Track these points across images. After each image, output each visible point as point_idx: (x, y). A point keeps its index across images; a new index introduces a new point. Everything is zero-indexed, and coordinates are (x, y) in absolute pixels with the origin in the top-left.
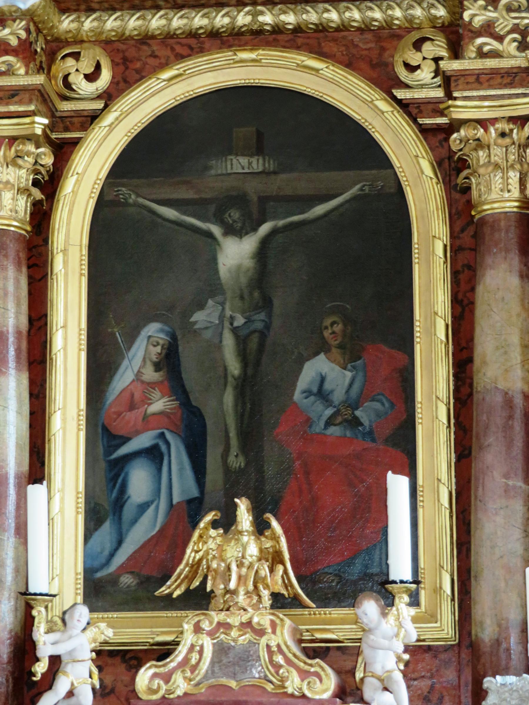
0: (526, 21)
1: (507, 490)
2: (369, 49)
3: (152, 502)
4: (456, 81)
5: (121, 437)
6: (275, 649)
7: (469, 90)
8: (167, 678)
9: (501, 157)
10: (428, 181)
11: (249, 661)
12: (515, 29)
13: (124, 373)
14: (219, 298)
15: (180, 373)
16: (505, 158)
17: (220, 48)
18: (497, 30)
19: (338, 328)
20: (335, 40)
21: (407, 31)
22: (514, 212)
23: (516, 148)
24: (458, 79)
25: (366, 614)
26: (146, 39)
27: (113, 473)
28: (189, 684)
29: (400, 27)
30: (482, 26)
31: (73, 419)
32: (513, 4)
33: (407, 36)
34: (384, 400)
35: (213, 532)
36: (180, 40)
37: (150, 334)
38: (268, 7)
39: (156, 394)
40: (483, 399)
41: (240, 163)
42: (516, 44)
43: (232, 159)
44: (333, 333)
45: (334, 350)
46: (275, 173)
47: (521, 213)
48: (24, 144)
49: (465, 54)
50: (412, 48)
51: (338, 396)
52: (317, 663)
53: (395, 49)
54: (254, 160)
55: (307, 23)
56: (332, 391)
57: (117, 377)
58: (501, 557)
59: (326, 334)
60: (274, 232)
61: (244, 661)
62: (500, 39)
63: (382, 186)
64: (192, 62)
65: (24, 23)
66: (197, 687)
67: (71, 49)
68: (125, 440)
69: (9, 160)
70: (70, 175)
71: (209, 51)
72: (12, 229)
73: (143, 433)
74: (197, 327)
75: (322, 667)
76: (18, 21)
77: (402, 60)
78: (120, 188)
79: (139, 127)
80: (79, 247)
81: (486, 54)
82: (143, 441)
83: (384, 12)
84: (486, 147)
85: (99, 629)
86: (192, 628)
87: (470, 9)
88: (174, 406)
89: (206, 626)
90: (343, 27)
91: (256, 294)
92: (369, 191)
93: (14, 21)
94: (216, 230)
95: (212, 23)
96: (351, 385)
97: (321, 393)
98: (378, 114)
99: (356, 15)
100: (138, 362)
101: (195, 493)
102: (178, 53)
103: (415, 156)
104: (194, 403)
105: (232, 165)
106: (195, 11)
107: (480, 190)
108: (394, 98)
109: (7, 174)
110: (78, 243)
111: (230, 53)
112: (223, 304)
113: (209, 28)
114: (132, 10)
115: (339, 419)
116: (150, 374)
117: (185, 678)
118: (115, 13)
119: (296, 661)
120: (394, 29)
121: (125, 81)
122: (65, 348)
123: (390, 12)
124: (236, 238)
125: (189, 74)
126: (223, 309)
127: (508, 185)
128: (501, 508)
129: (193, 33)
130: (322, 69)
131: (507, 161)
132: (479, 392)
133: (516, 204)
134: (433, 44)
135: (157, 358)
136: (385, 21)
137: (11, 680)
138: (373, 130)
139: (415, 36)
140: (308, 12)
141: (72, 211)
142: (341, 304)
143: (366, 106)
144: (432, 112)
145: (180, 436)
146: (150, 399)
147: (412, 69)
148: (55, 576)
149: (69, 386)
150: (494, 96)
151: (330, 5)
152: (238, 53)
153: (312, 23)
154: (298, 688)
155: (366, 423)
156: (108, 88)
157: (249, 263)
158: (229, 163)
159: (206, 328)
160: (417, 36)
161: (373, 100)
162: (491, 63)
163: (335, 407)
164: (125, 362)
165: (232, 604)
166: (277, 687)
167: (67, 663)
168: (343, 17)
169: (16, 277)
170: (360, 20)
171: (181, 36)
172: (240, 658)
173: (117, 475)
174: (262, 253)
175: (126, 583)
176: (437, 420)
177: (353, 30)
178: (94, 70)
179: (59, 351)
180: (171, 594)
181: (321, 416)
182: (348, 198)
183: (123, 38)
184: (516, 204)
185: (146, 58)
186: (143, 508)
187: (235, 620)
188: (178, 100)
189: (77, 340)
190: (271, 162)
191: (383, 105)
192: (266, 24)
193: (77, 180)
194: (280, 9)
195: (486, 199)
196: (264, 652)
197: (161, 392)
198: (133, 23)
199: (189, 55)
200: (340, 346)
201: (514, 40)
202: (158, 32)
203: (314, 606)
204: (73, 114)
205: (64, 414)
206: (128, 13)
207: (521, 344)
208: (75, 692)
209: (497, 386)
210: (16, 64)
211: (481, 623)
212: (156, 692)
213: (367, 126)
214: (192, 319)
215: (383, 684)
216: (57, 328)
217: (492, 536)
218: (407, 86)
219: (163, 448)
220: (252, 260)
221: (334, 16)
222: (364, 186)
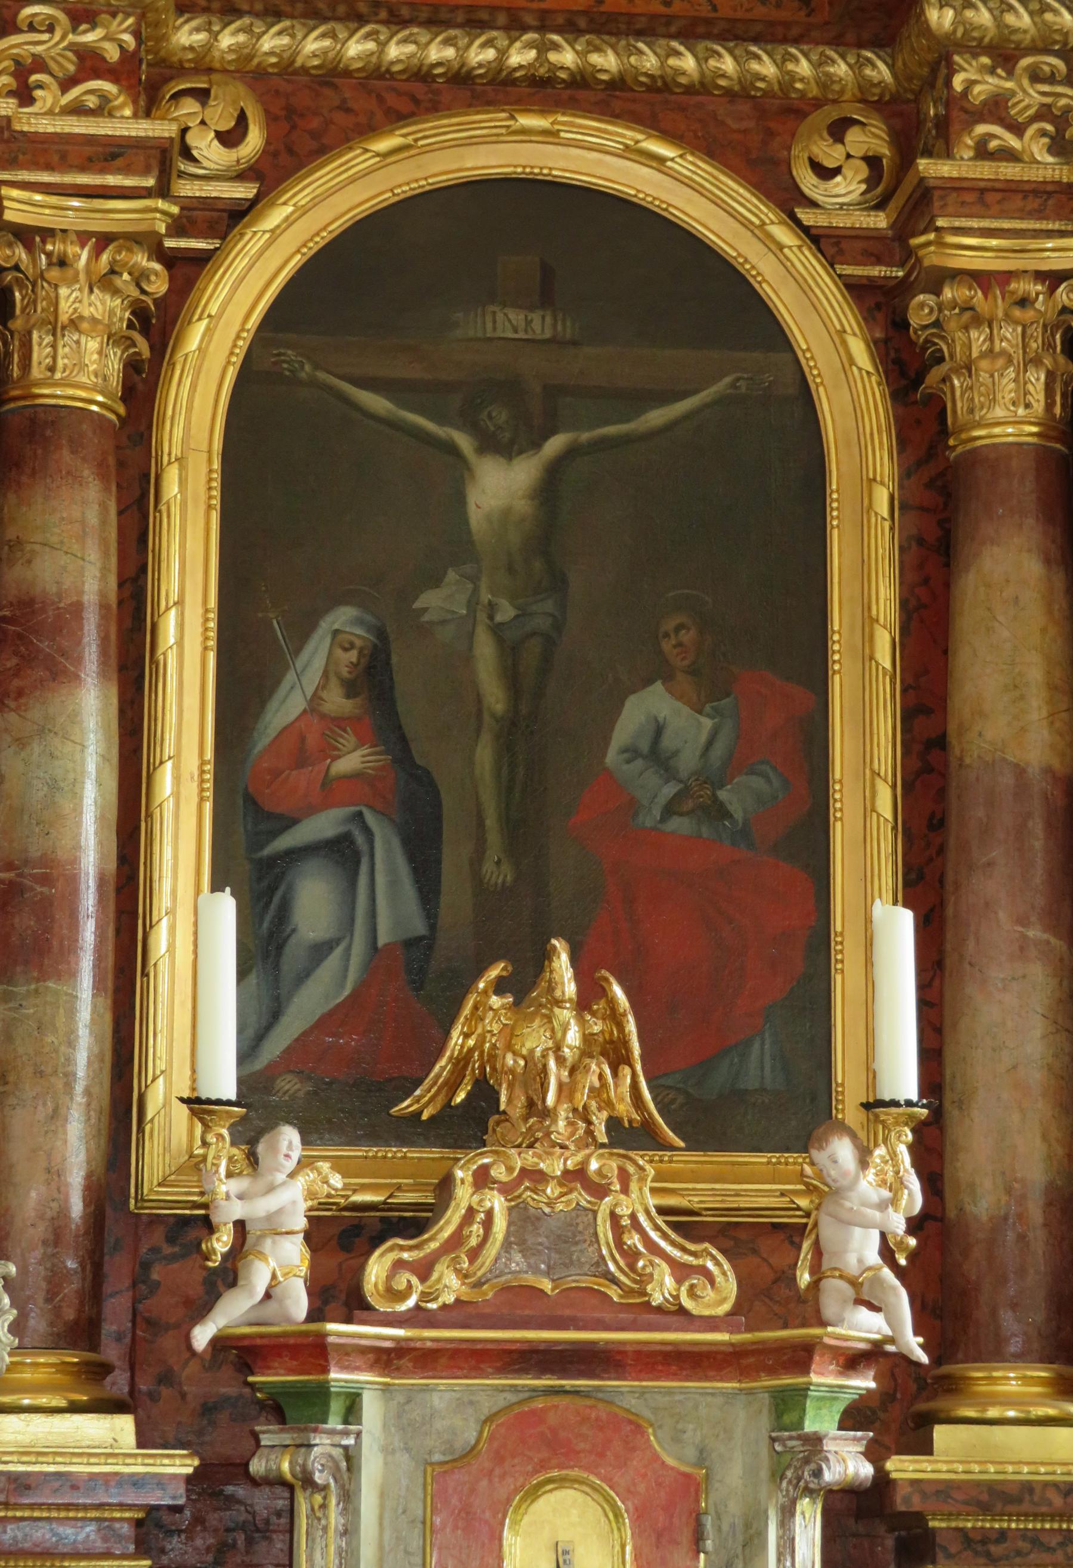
0: (1063, 102)
1: (1023, 946)
2: (745, 131)
3: (337, 941)
4: (942, 198)
5: (280, 817)
6: (626, 1222)
7: (966, 216)
8: (424, 1270)
9: (1014, 342)
10: (862, 378)
11: (577, 1243)
12: (1044, 113)
13: (286, 697)
14: (468, 568)
15: (393, 702)
16: (1021, 345)
17: (470, 106)
18: (1012, 112)
19: (687, 637)
20: (682, 109)
21: (814, 105)
22: (1028, 444)
23: (1040, 330)
24: (946, 196)
25: (835, 1162)
26: (332, 74)
27: (265, 884)
28: (463, 1284)
29: (802, 94)
30: (985, 103)
31: (192, 778)
32: (1042, 69)
33: (815, 114)
34: (771, 774)
35: (495, 1001)
36: (395, 84)
37: (336, 626)
38: (566, 36)
39: (348, 739)
40: (977, 779)
41: (510, 321)
42: (1046, 140)
43: (494, 313)
44: (680, 644)
45: (680, 677)
46: (575, 343)
47: (1044, 446)
48: (130, 250)
49: (955, 151)
50: (825, 134)
51: (688, 761)
52: (706, 1250)
53: (793, 135)
54: (536, 317)
55: (637, 72)
56: (676, 753)
57: (273, 705)
58: (1015, 1067)
59: (667, 646)
60: (571, 453)
61: (566, 1242)
62: (1018, 130)
63: (770, 382)
64: (431, 124)
65: (131, 21)
66: (476, 1290)
67: (190, 82)
68: (290, 822)
69: (94, 278)
70: (196, 317)
71: (449, 109)
72: (94, 408)
73: (322, 810)
74: (426, 618)
75: (714, 1258)
76: (120, 17)
77: (806, 155)
78: (282, 351)
79: (323, 238)
80: (205, 456)
81: (992, 154)
82: (322, 825)
83: (780, 66)
84: (986, 324)
85: (320, 1173)
86: (470, 1179)
87: (965, 70)
88: (381, 763)
89: (499, 1173)
90: (703, 87)
91: (538, 565)
92: (747, 389)
93: (114, 15)
94: (464, 442)
95: (462, 56)
96: (710, 743)
97: (655, 752)
98: (770, 249)
99: (728, 64)
100: (312, 677)
101: (419, 927)
102: (390, 108)
103: (838, 332)
104: (419, 761)
105: (494, 322)
106: (430, 32)
107: (972, 400)
108: (798, 222)
109: (90, 305)
110: (204, 446)
111: (503, 115)
112: (474, 579)
113: (456, 66)
114: (312, 19)
115: (689, 805)
116: (336, 702)
117: (458, 1272)
118: (279, 22)
119: (663, 1244)
120: (791, 98)
121: (290, 151)
122: (180, 643)
123: (790, 66)
124: (501, 460)
125: (422, 146)
126: (476, 590)
127: (1025, 395)
128: (1013, 979)
129: (423, 73)
130: (672, 160)
131: (1025, 352)
132: (969, 766)
133: (1034, 429)
134: (864, 131)
135: (350, 673)
136: (779, 82)
137: (88, 1267)
138: (759, 279)
139: (833, 113)
140: (641, 52)
141: (196, 386)
142: (694, 592)
143: (749, 233)
144: (862, 254)
145: (392, 820)
146: (336, 749)
147: (826, 173)
148: (158, 1072)
149: (186, 716)
150: (1008, 230)
151: (681, 43)
152: (517, 116)
153: (646, 74)
154: (670, 1295)
155: (739, 815)
156: (257, 161)
157: (523, 506)
158: (489, 319)
159: (443, 622)
160: (835, 116)
161: (764, 224)
162: (1009, 171)
163: (681, 782)
164: (290, 677)
165: (539, 1135)
166: (628, 1292)
167: (262, 1237)
168: (704, 66)
169: (104, 502)
170: (735, 76)
171: (399, 77)
172: (559, 1236)
173: (272, 889)
174: (549, 488)
175: (288, 1091)
176: (875, 815)
177: (716, 92)
178: (236, 125)
179: (171, 647)
180: (419, 1113)
181: (655, 796)
182: (709, 399)
183: (288, 68)
184: (1034, 429)
185: (330, 111)
186: (320, 951)
187: (555, 1166)
188: (398, 194)
189: (200, 630)
190: (568, 324)
191: (783, 234)
192: (562, 68)
193: (208, 329)
194: (588, 43)
195: (981, 418)
196: (605, 1227)
197: (356, 734)
198: (314, 45)
199: (413, 114)
200: (693, 671)
201: (1044, 133)
202: (360, 65)
203: (682, 1144)
204: (195, 204)
205: (177, 768)
206: (304, 25)
207: (1048, 684)
208: (277, 1292)
209: (1007, 757)
210: (116, 98)
211: (972, 1186)
212: (403, 1296)
213: (747, 270)
214: (417, 605)
215: (857, 1293)
216: (167, 603)
217: (995, 1030)
218: (813, 204)
219: (360, 839)
220: (529, 502)
221: (688, 63)
222: (738, 379)
